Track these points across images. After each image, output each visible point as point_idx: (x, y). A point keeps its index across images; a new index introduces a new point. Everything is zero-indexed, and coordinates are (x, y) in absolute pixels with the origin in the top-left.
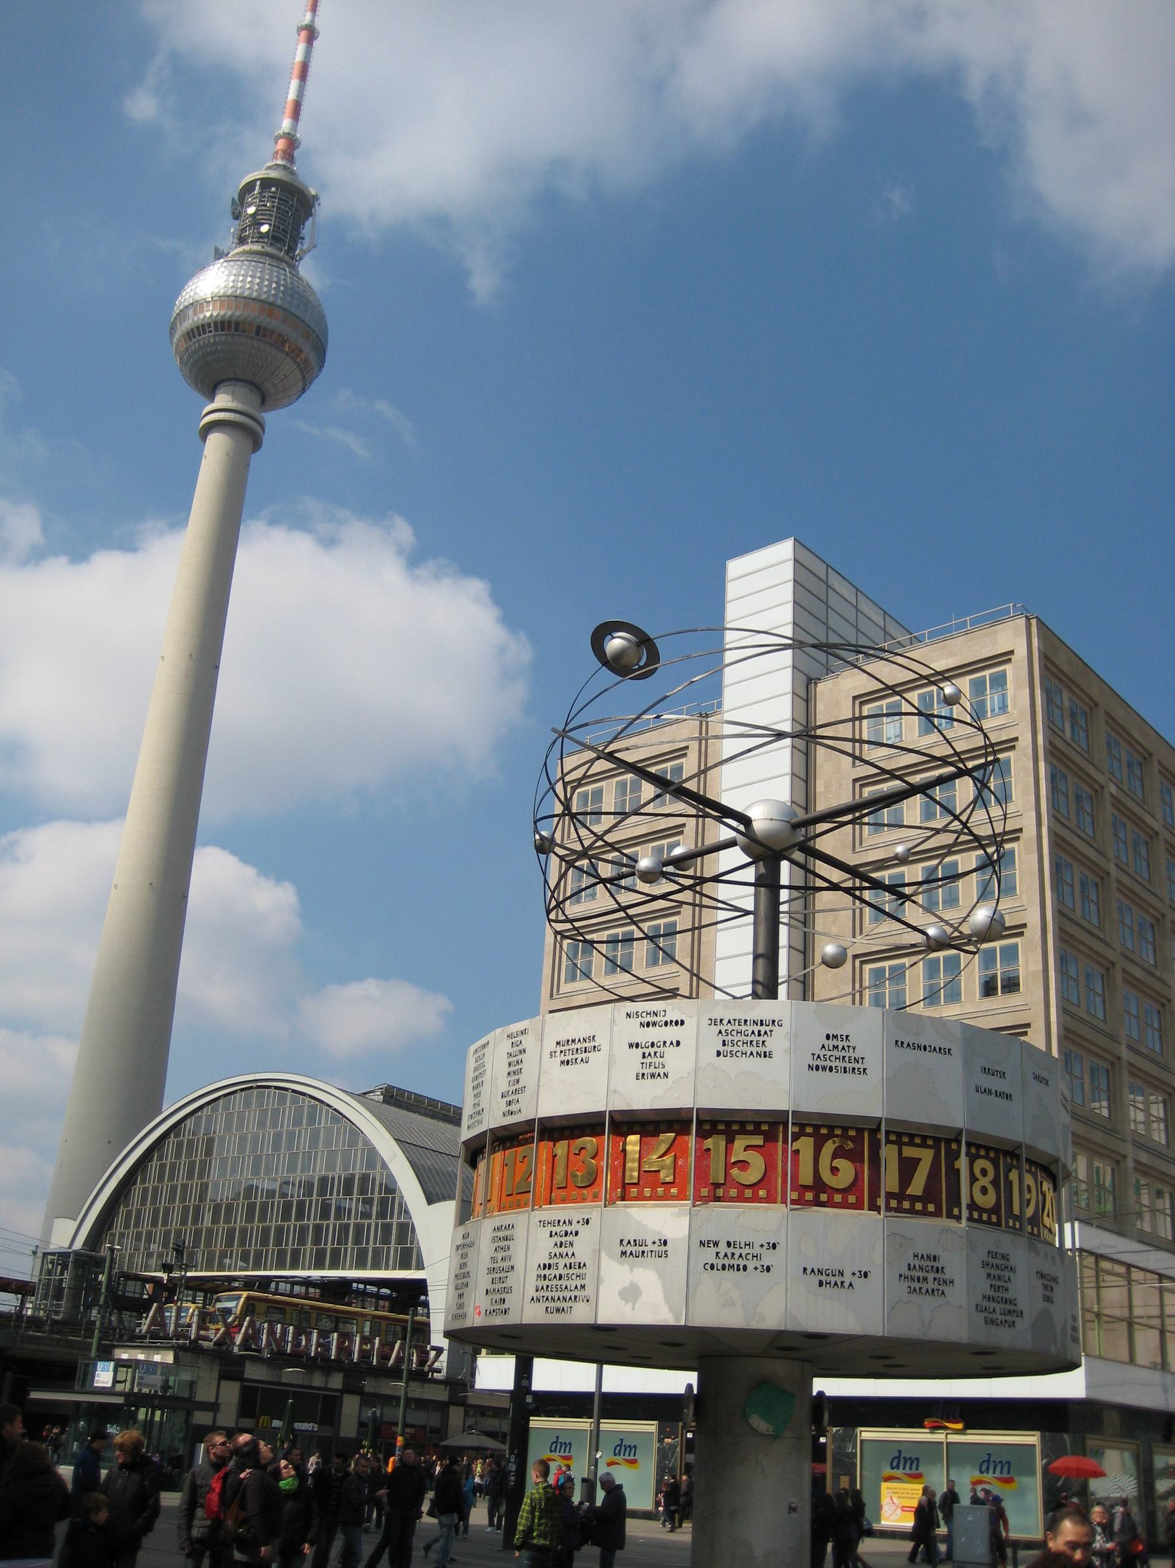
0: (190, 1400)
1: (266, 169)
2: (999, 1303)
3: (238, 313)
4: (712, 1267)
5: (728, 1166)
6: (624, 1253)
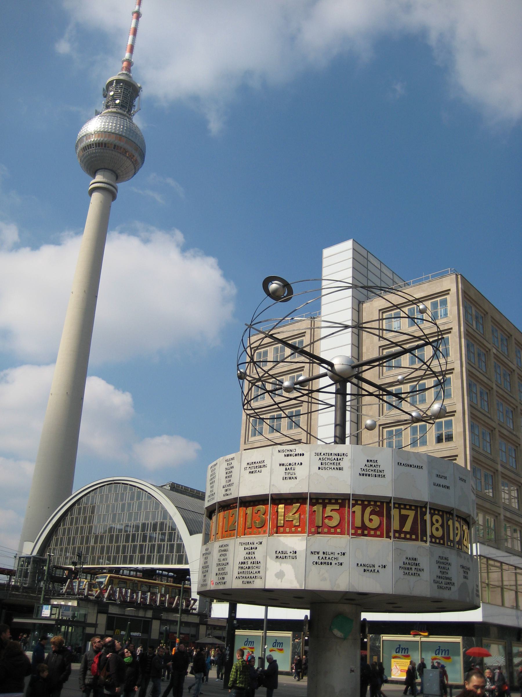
0: (84, 622)
1: (118, 75)
2: (444, 579)
3: (106, 139)
4: (316, 563)
5: (324, 518)
6: (277, 557)
